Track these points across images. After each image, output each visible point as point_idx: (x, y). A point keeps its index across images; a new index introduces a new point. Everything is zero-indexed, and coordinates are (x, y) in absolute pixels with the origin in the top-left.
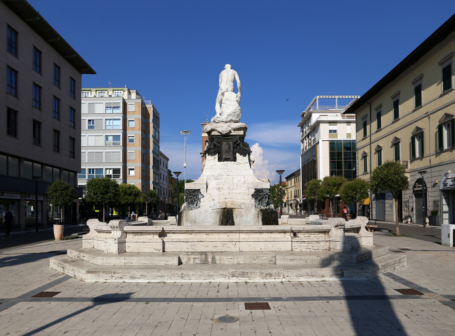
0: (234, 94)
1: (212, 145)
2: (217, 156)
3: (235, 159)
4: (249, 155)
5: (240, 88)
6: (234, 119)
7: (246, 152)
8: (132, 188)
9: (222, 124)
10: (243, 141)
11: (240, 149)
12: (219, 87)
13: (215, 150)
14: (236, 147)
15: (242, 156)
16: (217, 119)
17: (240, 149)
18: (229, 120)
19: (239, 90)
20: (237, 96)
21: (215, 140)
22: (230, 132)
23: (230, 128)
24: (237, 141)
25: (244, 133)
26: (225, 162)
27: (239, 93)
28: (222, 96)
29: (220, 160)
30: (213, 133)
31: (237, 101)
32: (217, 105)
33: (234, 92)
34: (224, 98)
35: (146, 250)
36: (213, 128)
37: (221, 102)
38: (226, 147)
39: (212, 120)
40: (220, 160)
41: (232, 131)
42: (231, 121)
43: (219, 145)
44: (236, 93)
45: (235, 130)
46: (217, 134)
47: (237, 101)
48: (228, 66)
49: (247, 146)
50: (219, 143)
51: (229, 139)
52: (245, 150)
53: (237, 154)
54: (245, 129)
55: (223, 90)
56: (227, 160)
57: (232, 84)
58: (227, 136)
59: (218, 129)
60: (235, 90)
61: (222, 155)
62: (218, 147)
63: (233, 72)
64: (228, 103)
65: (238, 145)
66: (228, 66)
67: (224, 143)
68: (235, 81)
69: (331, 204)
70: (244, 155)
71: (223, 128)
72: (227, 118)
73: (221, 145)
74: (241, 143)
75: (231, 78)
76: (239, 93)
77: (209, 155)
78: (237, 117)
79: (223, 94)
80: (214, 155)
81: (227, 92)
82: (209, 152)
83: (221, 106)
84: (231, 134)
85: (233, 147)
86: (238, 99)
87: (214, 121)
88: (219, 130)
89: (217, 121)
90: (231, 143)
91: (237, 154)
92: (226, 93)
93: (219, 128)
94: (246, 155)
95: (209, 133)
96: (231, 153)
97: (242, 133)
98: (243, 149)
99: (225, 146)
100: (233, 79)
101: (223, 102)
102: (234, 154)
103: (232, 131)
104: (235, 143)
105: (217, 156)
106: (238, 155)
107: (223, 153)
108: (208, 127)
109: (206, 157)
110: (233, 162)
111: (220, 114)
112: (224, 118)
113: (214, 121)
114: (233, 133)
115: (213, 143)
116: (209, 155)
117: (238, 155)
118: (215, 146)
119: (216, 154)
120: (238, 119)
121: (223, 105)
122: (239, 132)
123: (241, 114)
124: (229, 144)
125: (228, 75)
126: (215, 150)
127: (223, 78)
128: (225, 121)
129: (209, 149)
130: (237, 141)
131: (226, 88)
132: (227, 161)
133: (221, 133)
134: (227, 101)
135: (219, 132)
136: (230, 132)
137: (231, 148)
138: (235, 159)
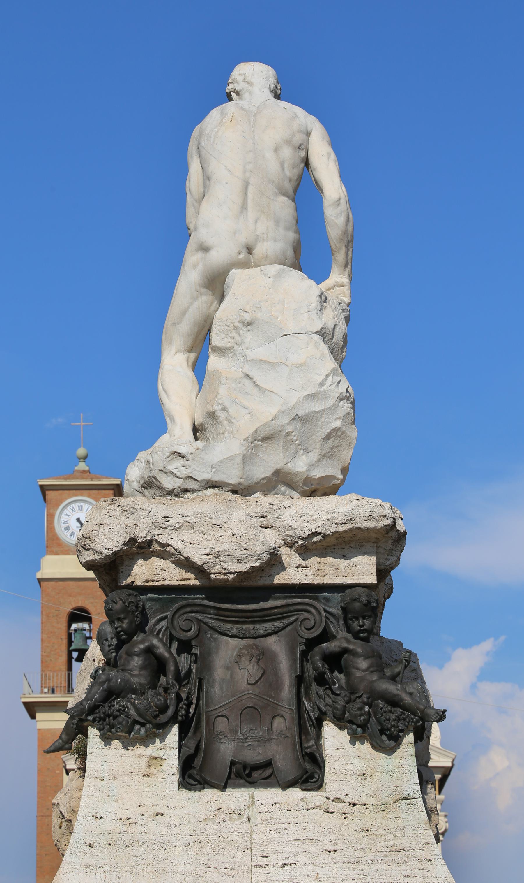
0: (298, 286)
1: (137, 662)
2: (169, 747)
3: (309, 773)
4: (422, 736)
5: (350, 241)
6: (301, 465)
7: (396, 715)
8: (192, 650)
9: (210, 504)
10: (373, 631)
11: (352, 689)
12: (186, 233)
13: (153, 698)
14: (321, 680)
15: (366, 747)
16: (176, 466)
17: (352, 689)
18: (261, 471)
19: (340, 257)
20: (323, 299)
21: (158, 622)
22: (274, 561)
23: (272, 539)
24: (326, 636)
25: (383, 573)
26: (238, 796)
27: (338, 277)
28: (206, 298)
29: (193, 774)
30: (142, 572)
31: (322, 333)
32: (174, 366)
33: (297, 266)
34: (226, 313)
35: (201, 702)
36: (142, 534)
37: (201, 344)
38: (247, 673)
39: (134, 473)
40: (193, 774)
41: (290, 558)
42: (279, 481)
43: (184, 659)
44: (319, 275)
45: (313, 546)
46: (172, 575)
47: (322, 333)
48: (254, 77)
49: (404, 665)
50: (185, 647)
51: (263, 617)
52: (394, 702)
53: (329, 730)
54: (386, 543)
55: (219, 256)
56: (248, 774)
57: (284, 207)
58: (244, 596)
59: (176, 541)
60: (307, 255)
61: (213, 737)
62: (181, 679)
63: (291, 117)
64: (255, 348)
65: (335, 661)
66: (254, 77)
67: (227, 650)
68: (303, 188)
69: (267, 618)
70: (386, 740)
71: (223, 537)
72: (246, 459)
73: (205, 662)
74: (357, 647)
75: (278, 165)
76: (338, 277)
77: (107, 739)
78: (327, 456)
79: (216, 284)
80: (146, 741)
81: (245, 265)
82: (109, 714)
83: (199, 368)
84: (279, 579)
85: (300, 680)
86: (331, 317)
87: (149, 485)
88: (188, 552)
89: (169, 483)
90: (275, 644)
91: (329, 730)
92: (236, 276)
93: (187, 535)
94: (396, 740)
95: (110, 569)
96: (278, 724)
97: (362, 569)
98: (375, 696)
99: (230, 664)
100: (291, 172)
101: (216, 340)
102: (302, 729)
103: (290, 558)
104: (311, 644)
105: (169, 747)
106: (333, 738)
107: (221, 725)
108: (89, 524)
109: (82, 754)
110: (296, 793)
111: (196, 430)
112: (221, 457)
113: (149, 485)
114: (296, 572)
115: (140, 642)
116: (107, 739)
117: (333, 738)
118: (157, 666)
119: (165, 726)
120: (331, 470)
121: (214, 362)
122: (343, 563)
123: (353, 433)
124: (264, 657)
125: (252, 136)
126: (153, 698)
127: (217, 169)
128: (233, 477)
129: (110, 694)
130: (326, 636)
131: (243, 238)
132: (252, 783)
133: (200, 571)
134: (248, 337)
135: (186, 564)
136: (274, 561)
137: (277, 686)
138: (309, 773)
